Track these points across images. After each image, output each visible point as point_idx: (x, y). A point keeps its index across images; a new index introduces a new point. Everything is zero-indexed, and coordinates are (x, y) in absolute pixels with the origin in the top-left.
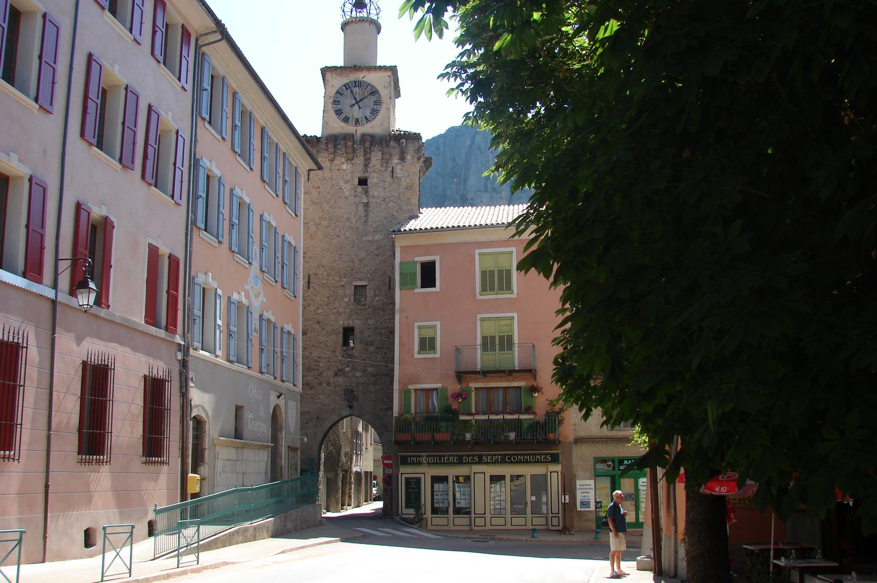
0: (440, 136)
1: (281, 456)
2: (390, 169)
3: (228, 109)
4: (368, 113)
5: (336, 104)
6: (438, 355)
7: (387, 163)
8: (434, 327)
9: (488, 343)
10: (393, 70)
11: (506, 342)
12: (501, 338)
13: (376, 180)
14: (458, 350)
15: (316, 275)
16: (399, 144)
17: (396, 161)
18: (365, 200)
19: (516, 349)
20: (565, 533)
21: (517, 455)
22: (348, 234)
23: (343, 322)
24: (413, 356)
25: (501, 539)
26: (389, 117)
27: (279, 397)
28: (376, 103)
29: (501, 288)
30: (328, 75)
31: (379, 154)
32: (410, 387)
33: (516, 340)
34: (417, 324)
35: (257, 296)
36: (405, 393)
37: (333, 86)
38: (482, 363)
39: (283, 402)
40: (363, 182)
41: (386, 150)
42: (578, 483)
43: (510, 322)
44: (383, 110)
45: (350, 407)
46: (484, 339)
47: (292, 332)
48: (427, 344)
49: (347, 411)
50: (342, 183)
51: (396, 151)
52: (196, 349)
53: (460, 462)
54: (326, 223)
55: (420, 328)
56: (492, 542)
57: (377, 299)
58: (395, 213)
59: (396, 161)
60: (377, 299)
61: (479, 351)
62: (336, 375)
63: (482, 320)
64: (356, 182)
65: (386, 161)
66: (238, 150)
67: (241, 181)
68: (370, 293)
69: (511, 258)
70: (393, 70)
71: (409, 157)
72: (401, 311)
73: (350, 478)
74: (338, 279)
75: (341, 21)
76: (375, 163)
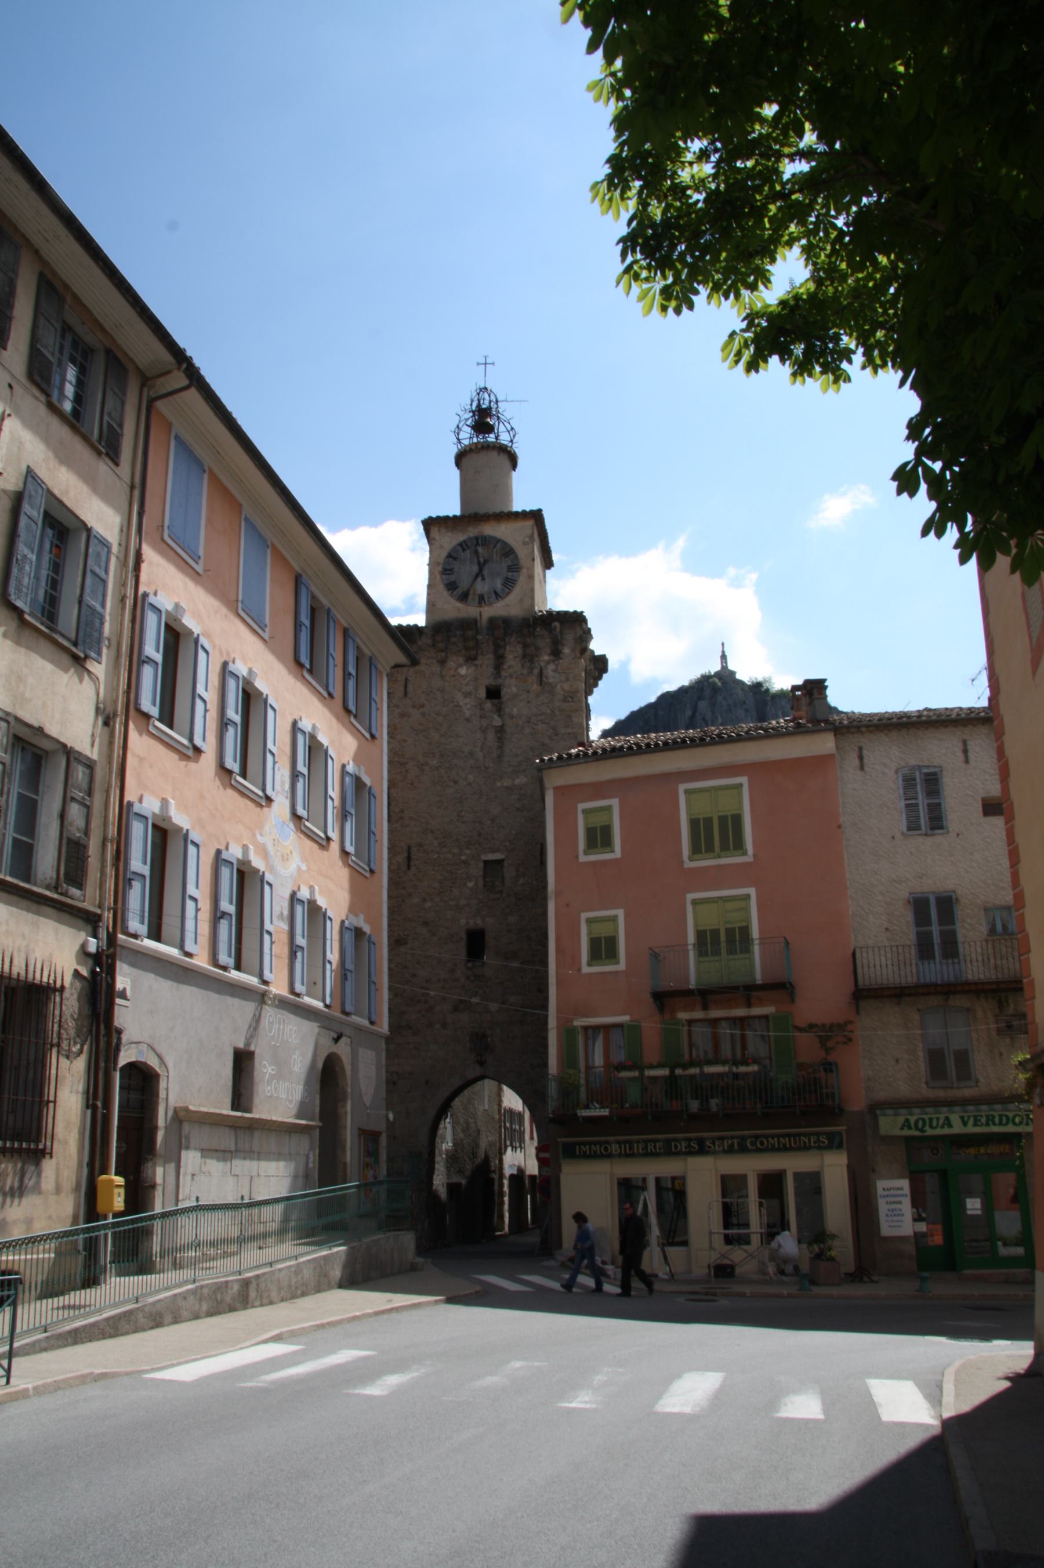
0: (650, 707)
1: (344, 1147)
2: (536, 671)
3: (337, 654)
4: (498, 584)
5: (445, 575)
6: (622, 966)
7: (531, 661)
8: (614, 919)
9: (707, 942)
10: (536, 517)
11: (739, 939)
12: (730, 932)
13: (514, 689)
14: (655, 955)
15: (420, 845)
16: (551, 630)
17: (546, 658)
18: (497, 721)
19: (756, 949)
20: (861, 1281)
21: (767, 1137)
22: (471, 778)
23: (465, 921)
24: (579, 970)
25: (743, 1295)
26: (532, 590)
27: (336, 1040)
28: (510, 569)
29: (725, 847)
30: (435, 531)
31: (519, 649)
32: (576, 1023)
33: (755, 933)
34: (584, 916)
35: (285, 858)
36: (568, 1034)
37: (441, 547)
38: (698, 972)
39: (348, 1050)
40: (494, 693)
41: (529, 640)
42: (881, 1185)
43: (743, 904)
44: (522, 579)
45: (481, 1063)
46: (700, 935)
47: (367, 929)
48: (603, 948)
49: (478, 1071)
50: (459, 697)
51: (544, 643)
52: (135, 936)
53: (669, 1151)
54: (435, 762)
55: (589, 921)
56: (723, 1302)
57: (521, 881)
58: (547, 741)
59: (546, 658)
60: (521, 881)
61: (692, 955)
62: (455, 1009)
63: (694, 902)
64: (483, 693)
65: (529, 658)
66: (352, 707)
67: (235, 646)
68: (509, 872)
69: (740, 794)
70: (536, 517)
71: (566, 651)
72: (558, 894)
73: (501, 1185)
74: (456, 850)
75: (454, 450)
76: (512, 663)
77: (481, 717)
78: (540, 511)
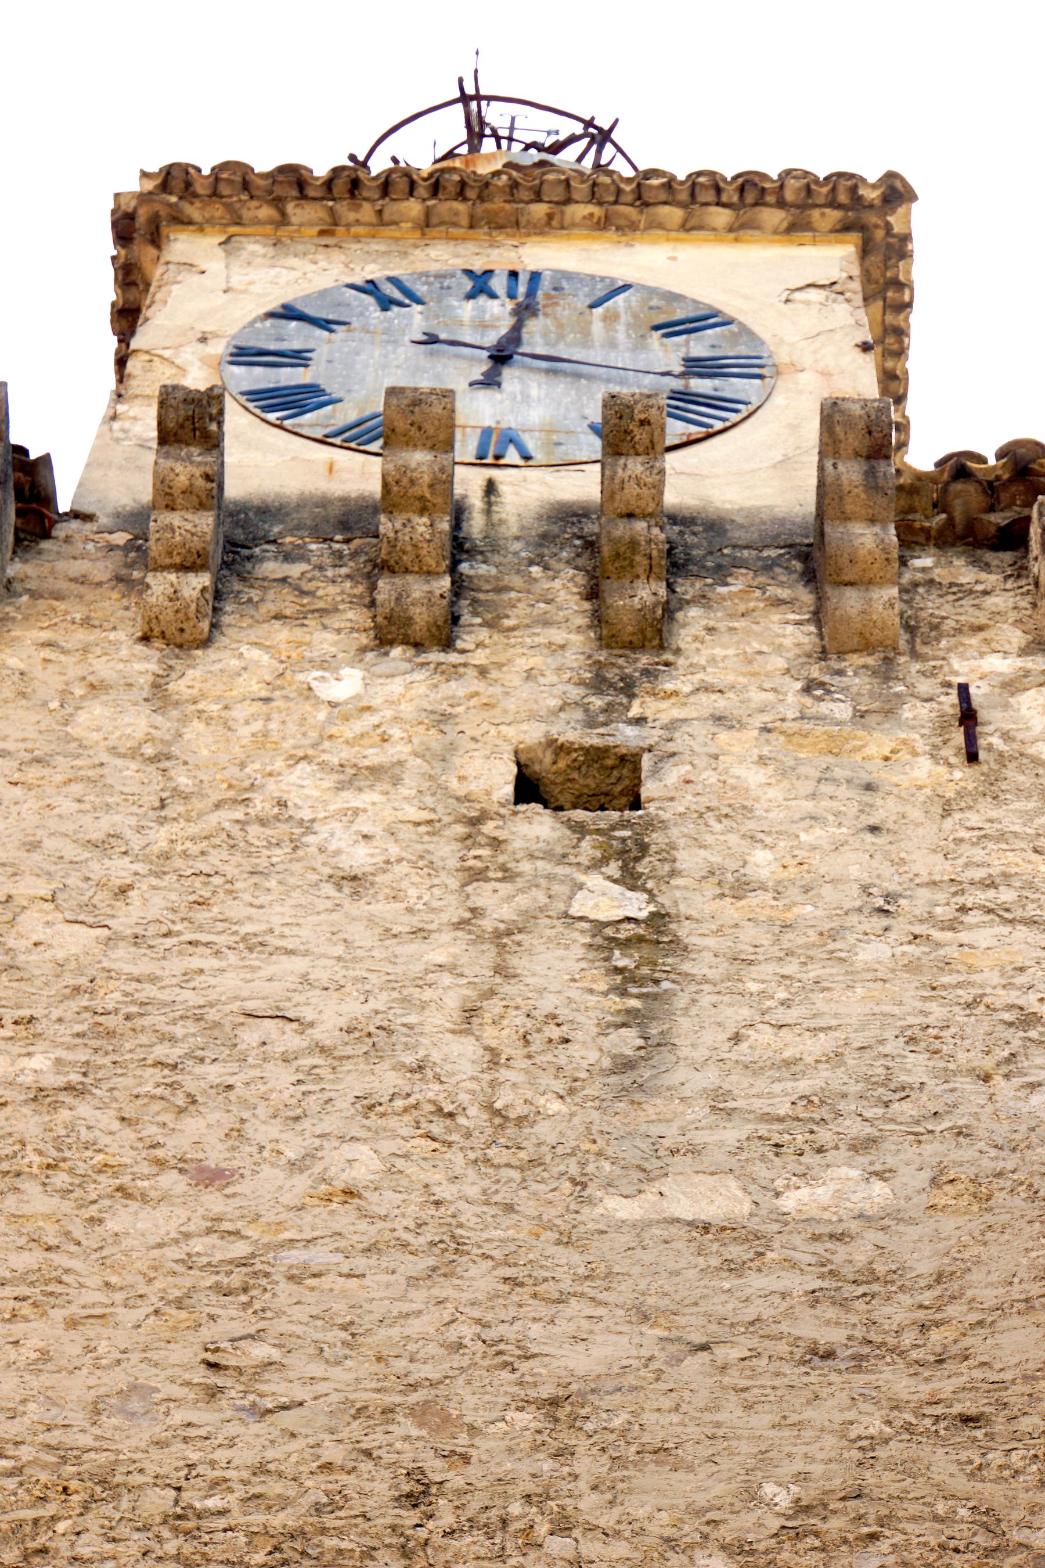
22: (361, 1164)
40: (588, 785)
77: (478, 875)
78: (896, 192)
